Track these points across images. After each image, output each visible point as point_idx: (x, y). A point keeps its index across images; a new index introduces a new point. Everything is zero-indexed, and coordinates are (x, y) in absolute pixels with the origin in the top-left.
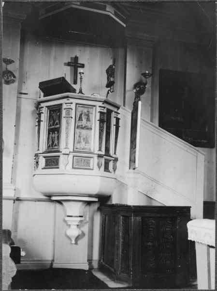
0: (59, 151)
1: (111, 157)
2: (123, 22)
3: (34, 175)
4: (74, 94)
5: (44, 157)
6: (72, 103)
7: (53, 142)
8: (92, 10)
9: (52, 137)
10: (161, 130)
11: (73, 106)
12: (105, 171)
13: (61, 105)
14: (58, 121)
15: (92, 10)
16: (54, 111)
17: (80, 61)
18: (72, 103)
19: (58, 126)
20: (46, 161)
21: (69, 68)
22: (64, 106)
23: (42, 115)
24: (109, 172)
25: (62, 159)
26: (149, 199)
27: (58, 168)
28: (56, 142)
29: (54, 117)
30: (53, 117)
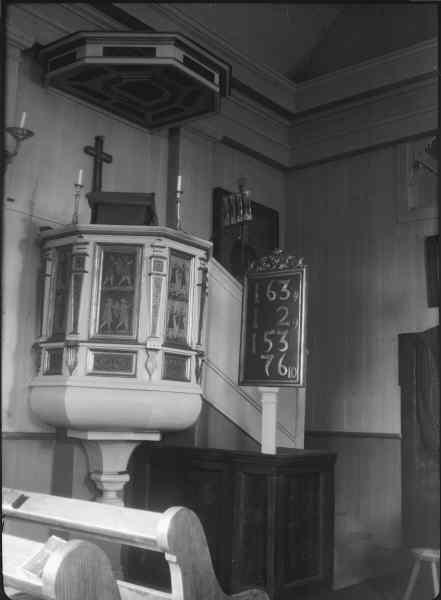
0: (136, 342)
1: (190, 349)
2: (187, 75)
3: (31, 388)
4: (155, 227)
5: (91, 350)
6: (164, 247)
7: (116, 320)
8: (203, 65)
9: (112, 310)
10: (157, 296)
11: (165, 253)
12: (166, 377)
13: (142, 246)
14: (128, 279)
15: (203, 65)
16: (117, 255)
17: (107, 149)
18: (164, 247)
19: (131, 288)
20: (97, 359)
21: (87, 157)
22: (148, 252)
23: (49, 264)
24: (184, 379)
25: (141, 358)
26: (243, 435)
27: (134, 376)
28: (124, 320)
29: (118, 268)
30: (114, 268)
